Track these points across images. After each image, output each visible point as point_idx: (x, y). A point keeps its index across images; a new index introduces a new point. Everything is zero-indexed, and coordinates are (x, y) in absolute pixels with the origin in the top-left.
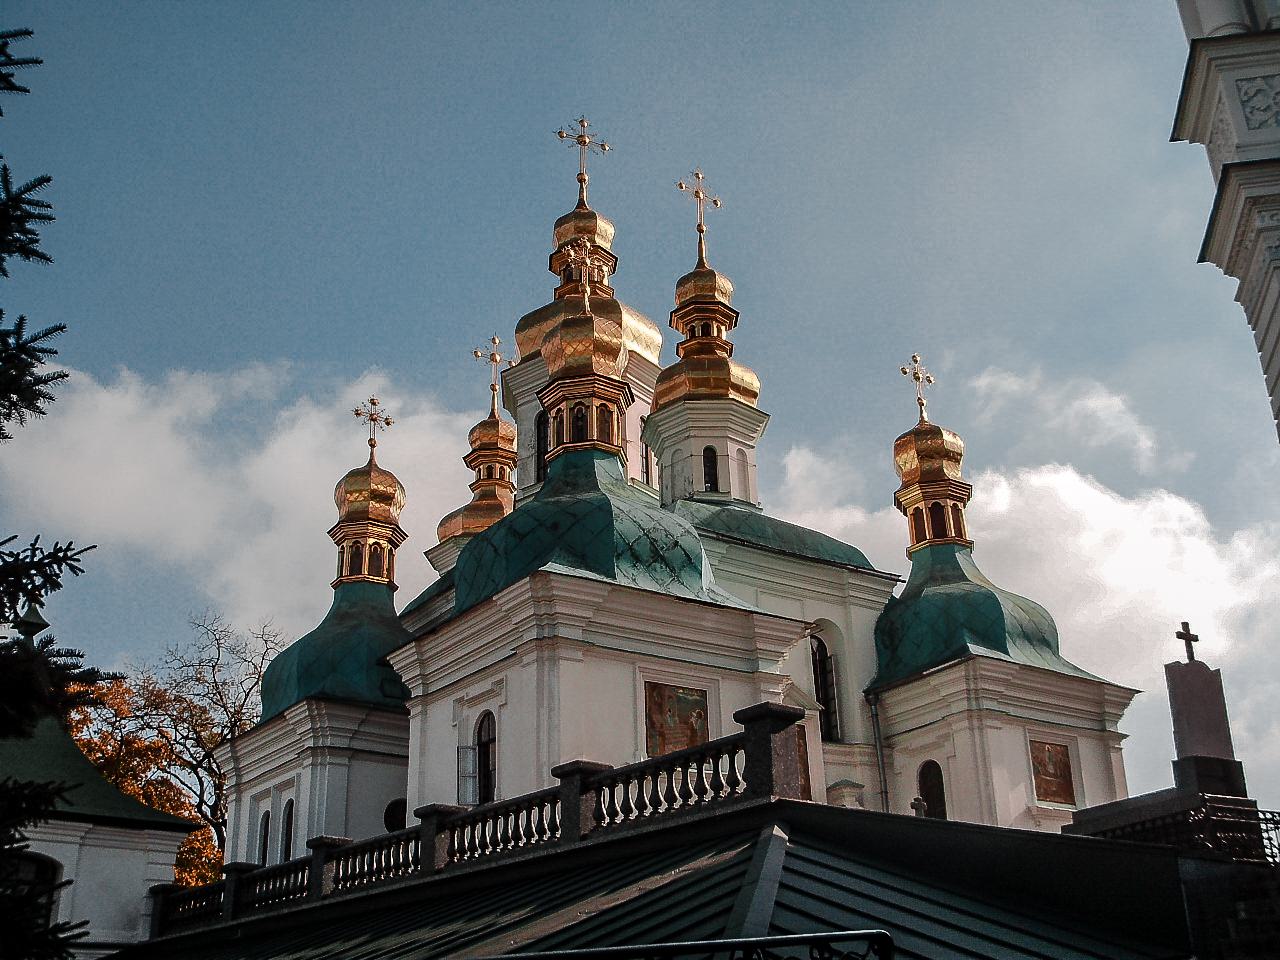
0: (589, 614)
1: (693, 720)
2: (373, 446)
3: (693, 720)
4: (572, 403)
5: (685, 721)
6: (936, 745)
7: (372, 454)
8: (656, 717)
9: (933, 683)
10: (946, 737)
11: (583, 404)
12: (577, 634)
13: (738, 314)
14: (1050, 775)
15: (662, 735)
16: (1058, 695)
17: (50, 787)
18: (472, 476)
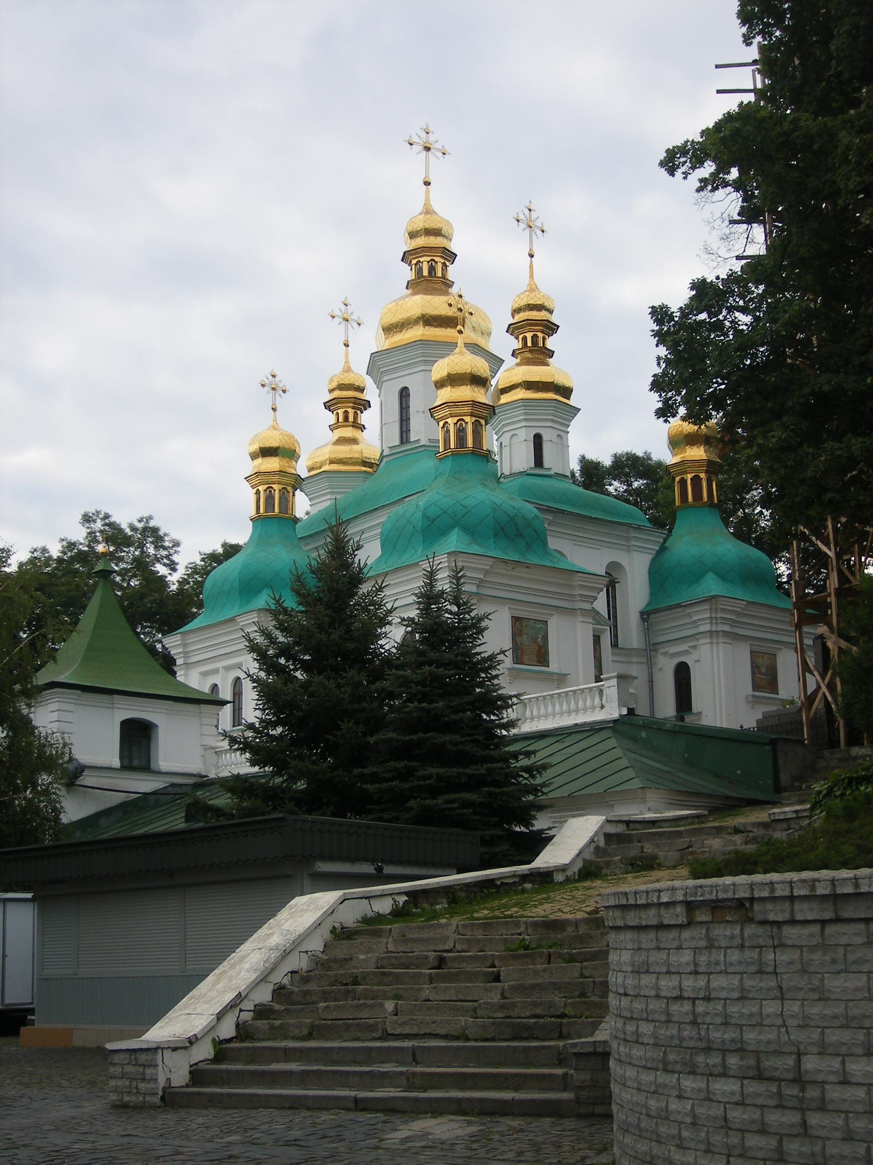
0: (733, 617)
1: (539, 640)
2: (531, 256)
3: (539, 640)
4: (455, 419)
5: (535, 640)
6: (687, 652)
7: (531, 267)
8: (518, 639)
9: (688, 611)
10: (695, 647)
11: (463, 420)
12: (707, 628)
13: (558, 327)
14: (762, 674)
15: (522, 649)
16: (544, 582)
17: (29, 895)
18: (331, 418)
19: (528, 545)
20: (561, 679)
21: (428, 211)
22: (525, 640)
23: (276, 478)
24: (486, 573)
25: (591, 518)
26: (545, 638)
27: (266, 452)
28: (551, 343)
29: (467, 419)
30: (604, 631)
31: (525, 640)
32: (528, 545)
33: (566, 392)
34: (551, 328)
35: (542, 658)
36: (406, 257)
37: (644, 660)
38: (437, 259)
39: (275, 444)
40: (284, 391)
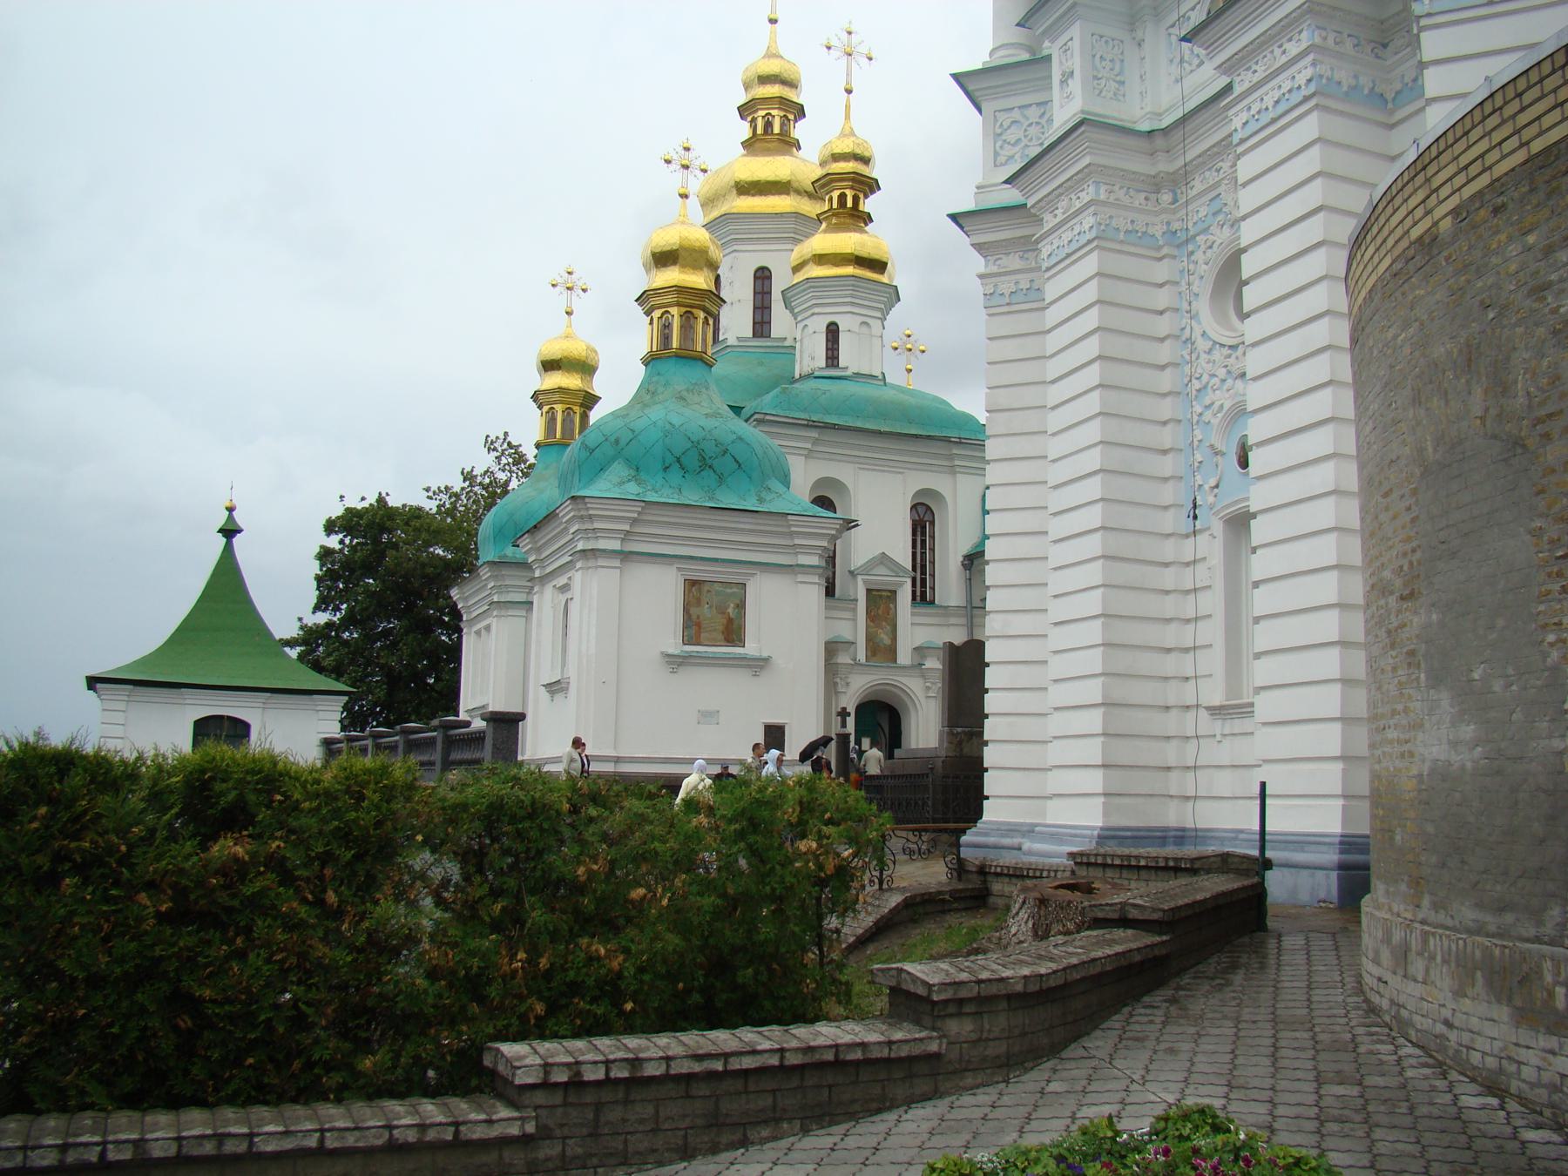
1: (730, 610)
3: (730, 610)
5: (722, 610)
7: (848, 108)
8: (694, 611)
12: (615, 545)
15: (699, 625)
19: (721, 479)
20: (759, 665)
21: (771, 55)
22: (705, 611)
23: (556, 397)
24: (634, 521)
25: (880, 433)
26: (741, 606)
27: (549, 366)
28: (869, 205)
29: (674, 311)
30: (901, 584)
31: (705, 611)
32: (721, 479)
33: (879, 266)
34: (868, 186)
35: (733, 633)
36: (745, 110)
37: (963, 621)
38: (774, 112)
39: (557, 356)
40: (584, 290)
